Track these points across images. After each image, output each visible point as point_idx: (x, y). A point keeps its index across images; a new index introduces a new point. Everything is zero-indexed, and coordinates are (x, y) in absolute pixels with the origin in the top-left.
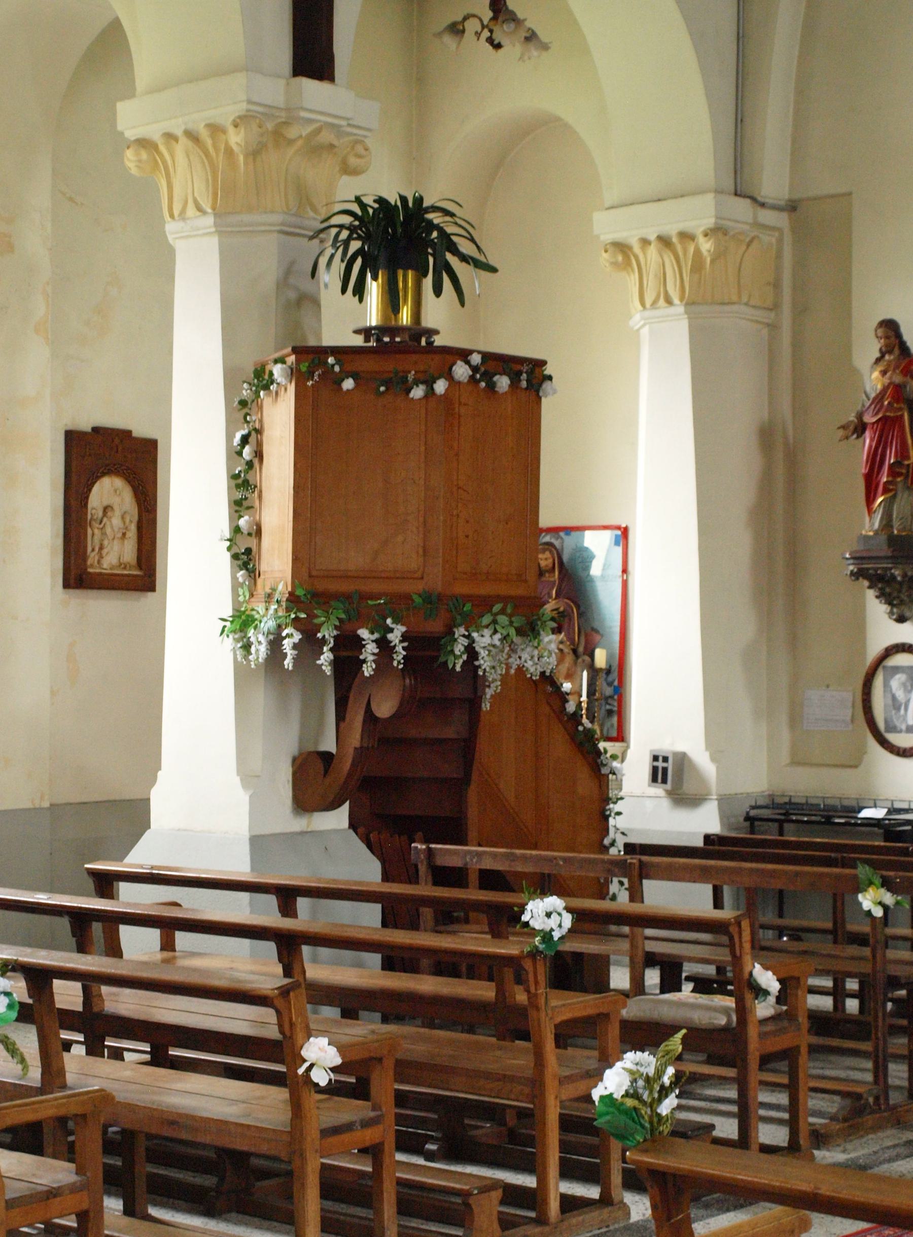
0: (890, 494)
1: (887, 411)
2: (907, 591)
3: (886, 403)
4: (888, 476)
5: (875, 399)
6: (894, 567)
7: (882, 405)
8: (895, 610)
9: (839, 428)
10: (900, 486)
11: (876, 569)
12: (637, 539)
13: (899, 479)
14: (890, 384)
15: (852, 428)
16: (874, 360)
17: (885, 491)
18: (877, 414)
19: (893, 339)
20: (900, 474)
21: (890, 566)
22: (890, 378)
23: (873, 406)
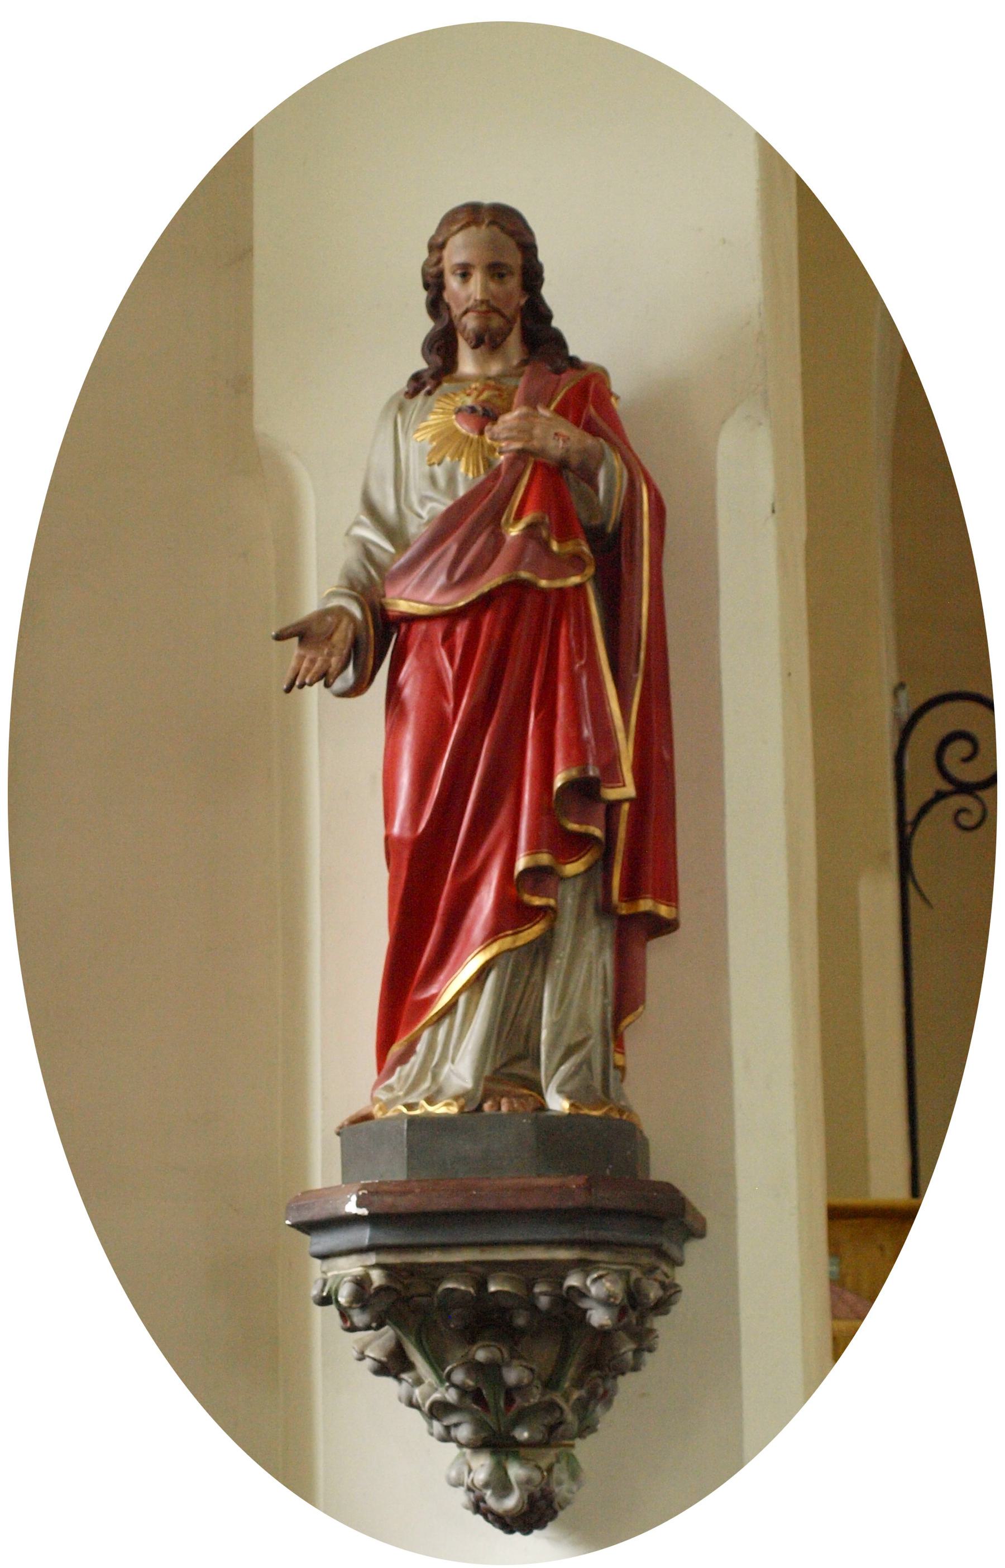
0: (532, 932)
1: (516, 563)
2: (579, 1383)
3: (514, 532)
4: (534, 848)
5: (446, 525)
6: (584, 1266)
7: (498, 539)
8: (515, 1471)
9: (280, 637)
10: (569, 899)
11: (480, 1274)
12: (344, 531)
13: (572, 869)
14: (521, 456)
15: (342, 636)
16: (402, 383)
17: (511, 914)
18: (472, 574)
19: (513, 283)
20: (579, 844)
21: (563, 1254)
22: (524, 431)
23: (451, 546)
